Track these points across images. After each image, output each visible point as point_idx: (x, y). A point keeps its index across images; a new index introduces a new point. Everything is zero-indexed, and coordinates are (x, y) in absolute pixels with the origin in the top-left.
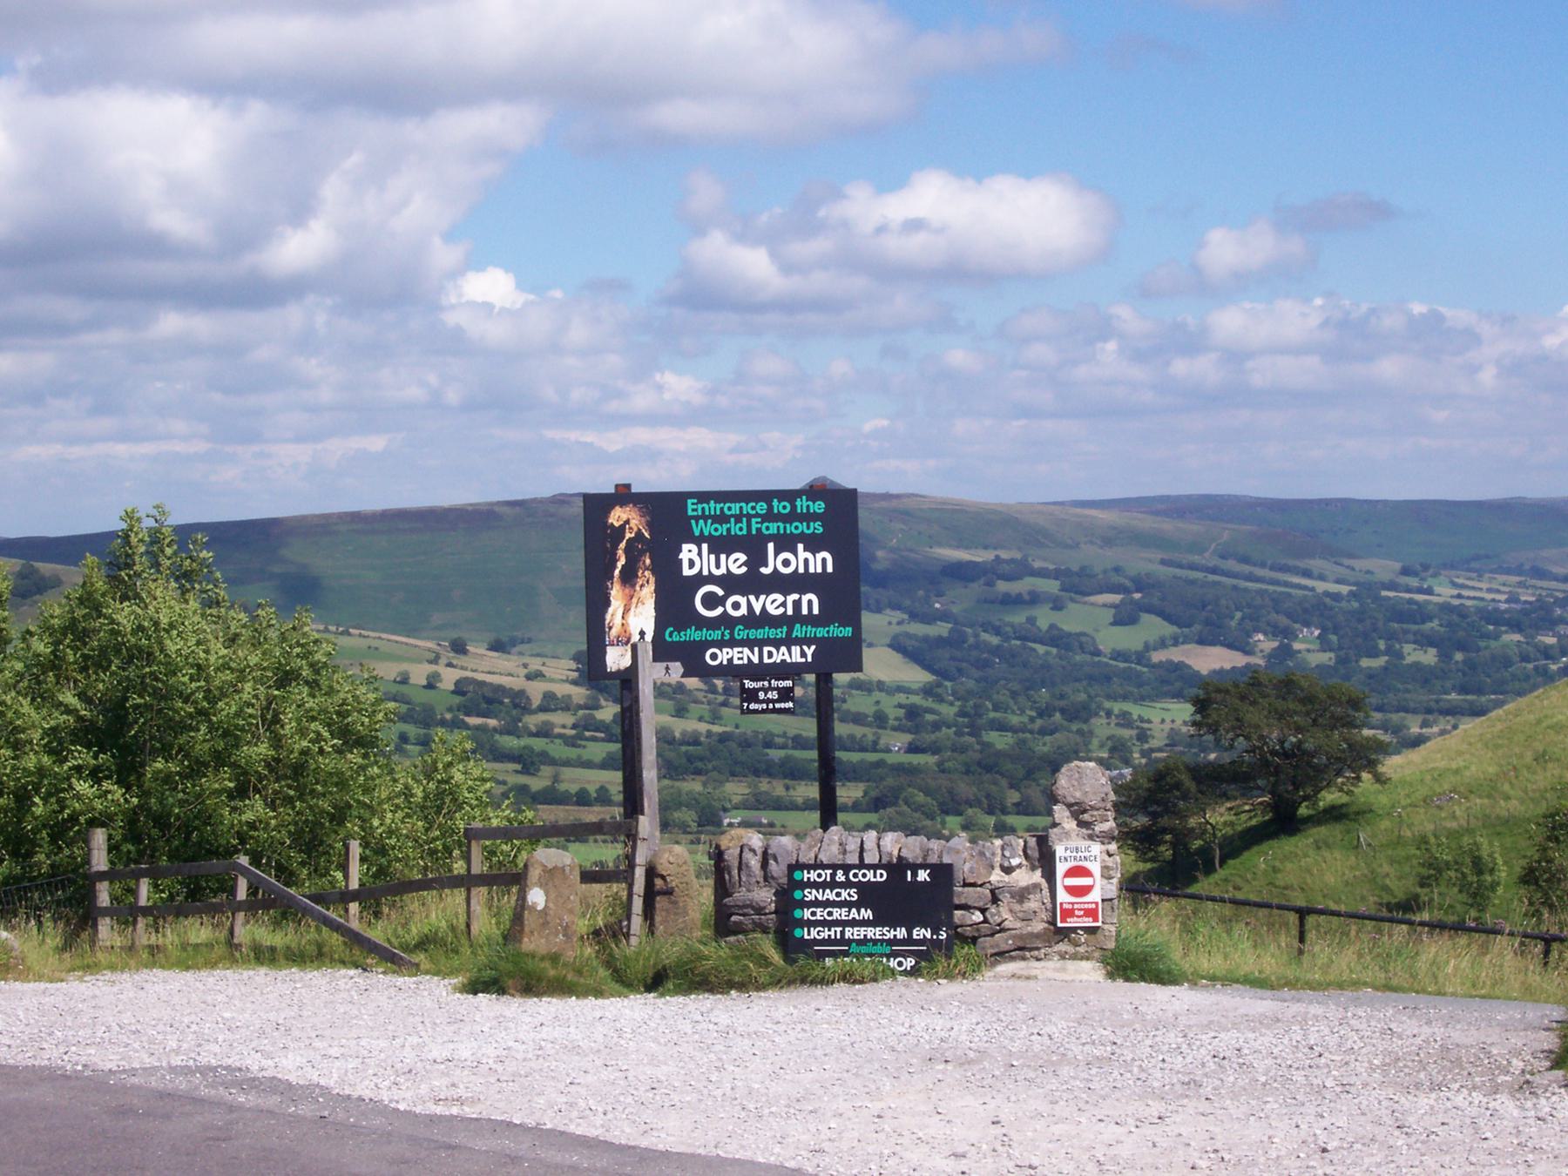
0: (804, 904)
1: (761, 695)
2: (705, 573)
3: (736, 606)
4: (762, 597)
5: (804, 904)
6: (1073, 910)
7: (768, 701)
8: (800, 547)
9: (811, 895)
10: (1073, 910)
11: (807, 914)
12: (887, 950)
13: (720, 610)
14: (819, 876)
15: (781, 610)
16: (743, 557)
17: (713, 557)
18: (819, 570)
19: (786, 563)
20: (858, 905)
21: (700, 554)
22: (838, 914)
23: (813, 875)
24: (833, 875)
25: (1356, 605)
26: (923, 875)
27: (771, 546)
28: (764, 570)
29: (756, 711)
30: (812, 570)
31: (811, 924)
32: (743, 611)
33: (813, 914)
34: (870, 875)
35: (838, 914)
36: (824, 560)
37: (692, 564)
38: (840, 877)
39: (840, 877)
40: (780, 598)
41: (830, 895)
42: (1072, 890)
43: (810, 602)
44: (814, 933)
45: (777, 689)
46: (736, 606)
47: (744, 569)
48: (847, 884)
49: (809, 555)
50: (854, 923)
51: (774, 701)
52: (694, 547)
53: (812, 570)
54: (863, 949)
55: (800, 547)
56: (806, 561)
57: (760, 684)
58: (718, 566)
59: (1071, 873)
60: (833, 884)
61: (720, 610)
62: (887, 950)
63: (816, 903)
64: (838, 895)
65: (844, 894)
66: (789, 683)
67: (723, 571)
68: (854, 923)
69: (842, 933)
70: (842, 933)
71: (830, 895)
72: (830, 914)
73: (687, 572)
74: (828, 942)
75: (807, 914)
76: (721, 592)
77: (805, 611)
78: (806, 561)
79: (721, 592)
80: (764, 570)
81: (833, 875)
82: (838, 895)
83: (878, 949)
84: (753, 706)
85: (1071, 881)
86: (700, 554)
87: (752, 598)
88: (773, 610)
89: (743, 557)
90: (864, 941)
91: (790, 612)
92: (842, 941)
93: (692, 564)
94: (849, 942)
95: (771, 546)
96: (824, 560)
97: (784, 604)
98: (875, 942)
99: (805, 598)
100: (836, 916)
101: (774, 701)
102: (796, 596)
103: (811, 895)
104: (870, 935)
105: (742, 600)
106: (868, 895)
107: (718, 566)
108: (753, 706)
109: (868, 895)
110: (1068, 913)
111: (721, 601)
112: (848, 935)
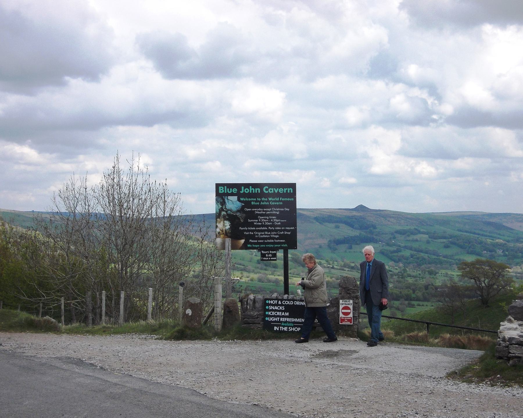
0: (269, 310)
1: (267, 255)
2: (226, 192)
5: (269, 310)
6: (344, 319)
7: (268, 257)
8: (251, 187)
9: (271, 308)
10: (344, 319)
11: (270, 313)
12: (292, 325)
14: (296, 329)
16: (236, 190)
20: (284, 311)
22: (279, 313)
23: (272, 302)
24: (278, 302)
29: (265, 260)
30: (254, 192)
33: (271, 313)
34: (288, 303)
35: (279, 313)
38: (280, 303)
39: (280, 303)
41: (276, 308)
42: (344, 313)
44: (271, 319)
45: (271, 254)
48: (282, 305)
49: (253, 189)
50: (283, 317)
51: (270, 257)
54: (286, 324)
55: (251, 187)
56: (252, 191)
57: (266, 252)
59: (343, 308)
60: (277, 305)
62: (292, 325)
63: (272, 310)
64: (279, 308)
65: (281, 308)
66: (275, 252)
68: (283, 317)
69: (280, 319)
70: (280, 319)
71: (276, 308)
72: (276, 313)
74: (275, 322)
75: (270, 313)
78: (252, 191)
81: (278, 302)
82: (279, 308)
83: (290, 325)
84: (264, 258)
85: (344, 311)
90: (286, 322)
92: (280, 322)
94: (282, 322)
98: (289, 322)
100: (278, 314)
101: (270, 257)
103: (271, 308)
104: (288, 320)
106: (288, 308)
108: (264, 258)
109: (288, 308)
110: (343, 320)
112: (281, 320)
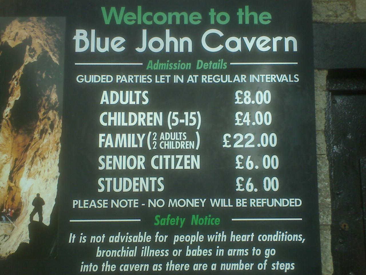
3: (233, 44)
4: (254, 39)
8: (168, 31)
13: (220, 47)
15: (268, 48)
16: (122, 40)
17: (99, 39)
18: (182, 50)
19: (156, 45)
21: (89, 37)
25: (331, 152)
26: (328, 144)
27: (145, 32)
28: (138, 50)
30: (176, 50)
31: (117, 174)
32: (239, 48)
36: (186, 43)
37: (82, 44)
40: (267, 39)
43: (291, 43)
46: (233, 44)
47: (123, 49)
52: (85, 32)
53: (176, 50)
58: (103, 46)
61: (220, 47)
67: (106, 49)
73: (78, 49)
76: (221, 34)
77: (287, 49)
79: (221, 34)
80: (138, 50)
86: (89, 37)
87: (246, 39)
88: (261, 48)
89: (122, 40)
91: (275, 49)
93: (82, 44)
95: (145, 32)
96: (186, 43)
97: (270, 44)
99: (287, 40)
102: (280, 38)
105: (238, 41)
107: (103, 46)
111: (222, 41)
